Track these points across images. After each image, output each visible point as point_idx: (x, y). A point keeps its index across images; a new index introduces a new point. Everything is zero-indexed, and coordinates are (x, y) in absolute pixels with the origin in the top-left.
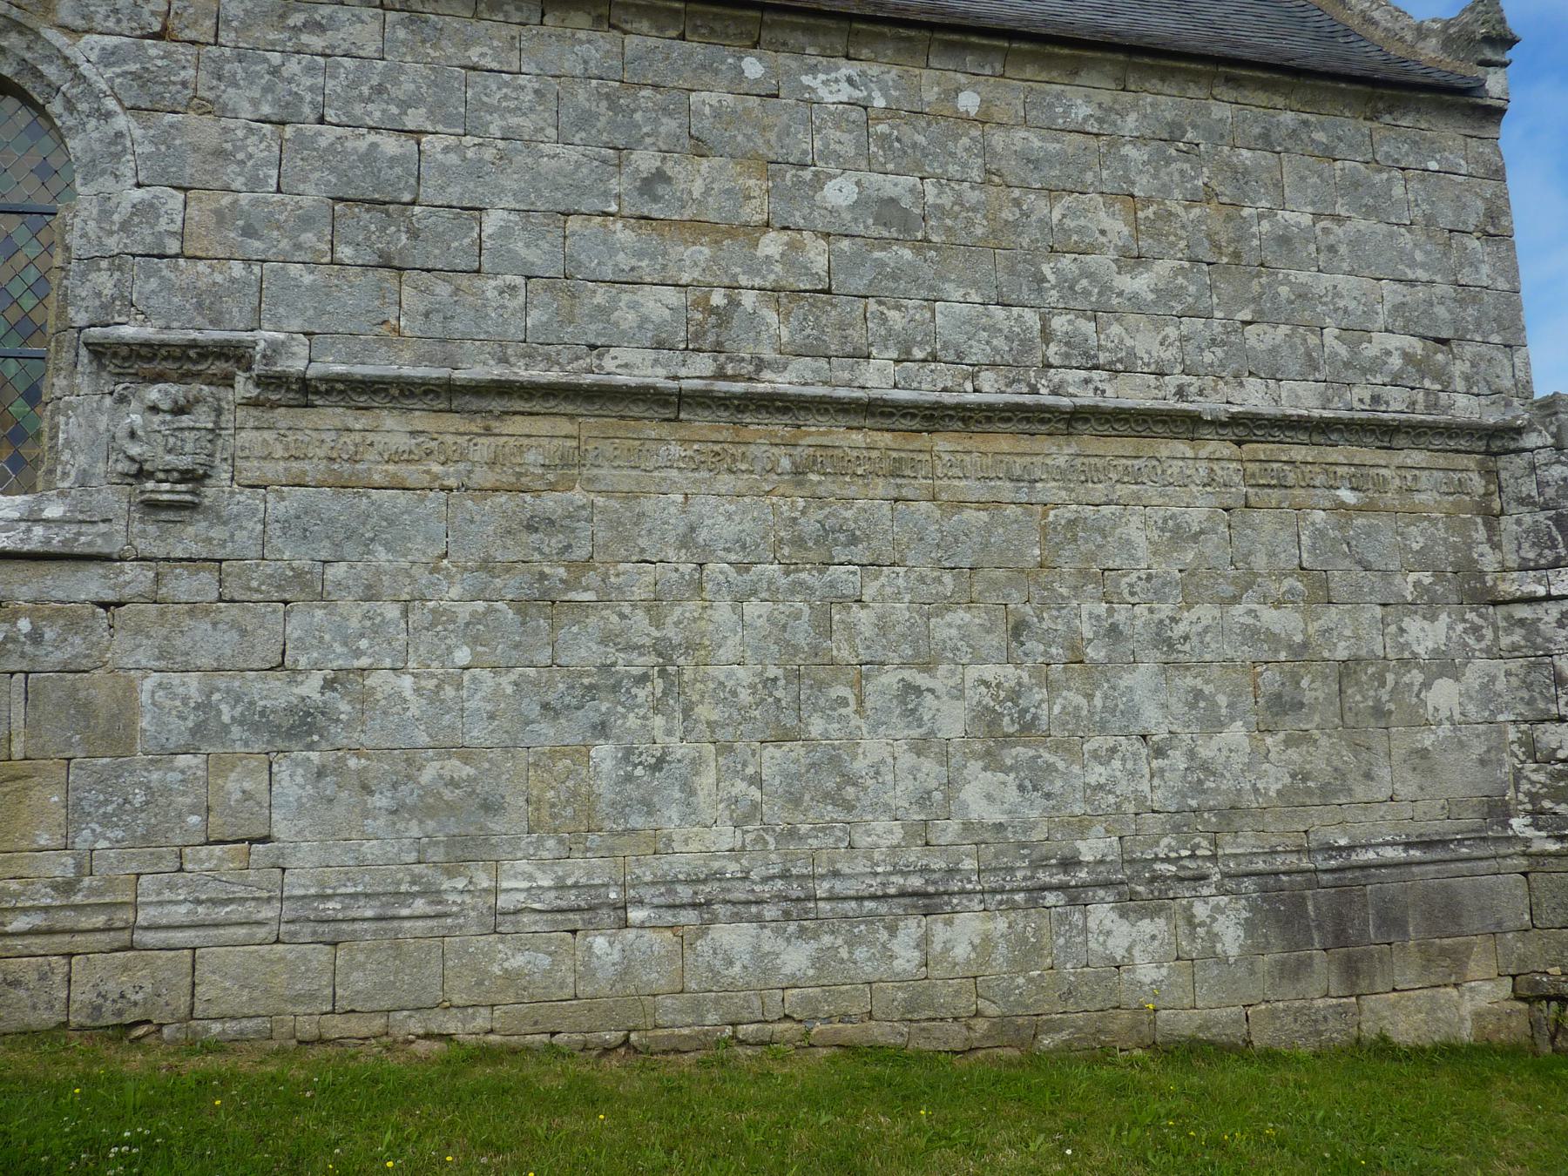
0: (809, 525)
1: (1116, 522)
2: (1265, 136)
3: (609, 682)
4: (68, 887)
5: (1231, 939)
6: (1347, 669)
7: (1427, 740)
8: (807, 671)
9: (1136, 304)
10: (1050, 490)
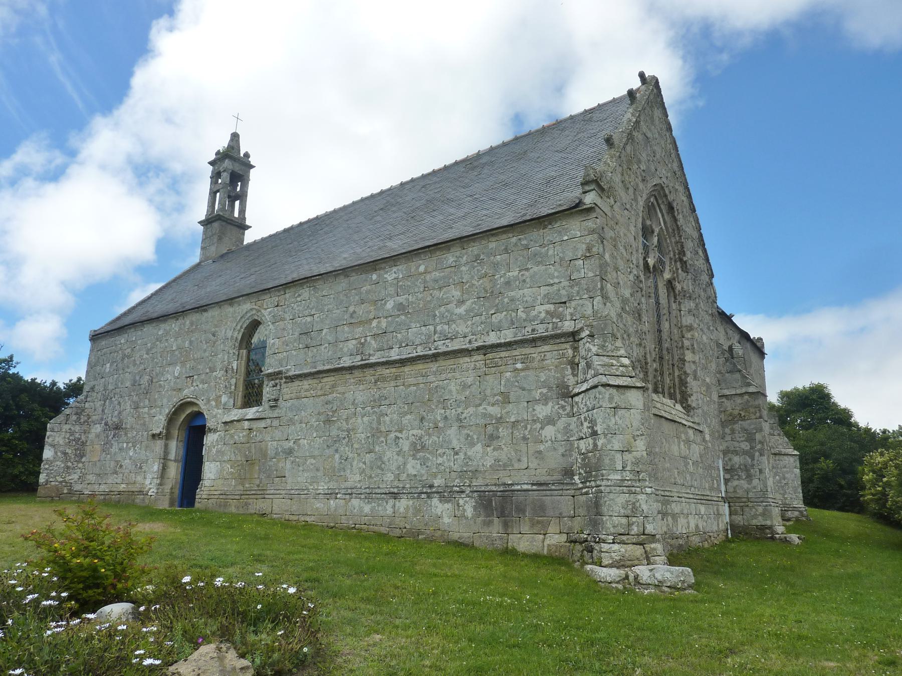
0: (377, 396)
1: (448, 384)
2: (506, 249)
3: (338, 440)
4: (258, 486)
5: (469, 512)
6: (515, 424)
7: (542, 447)
8: (376, 433)
9: (460, 317)
10: (431, 378)
